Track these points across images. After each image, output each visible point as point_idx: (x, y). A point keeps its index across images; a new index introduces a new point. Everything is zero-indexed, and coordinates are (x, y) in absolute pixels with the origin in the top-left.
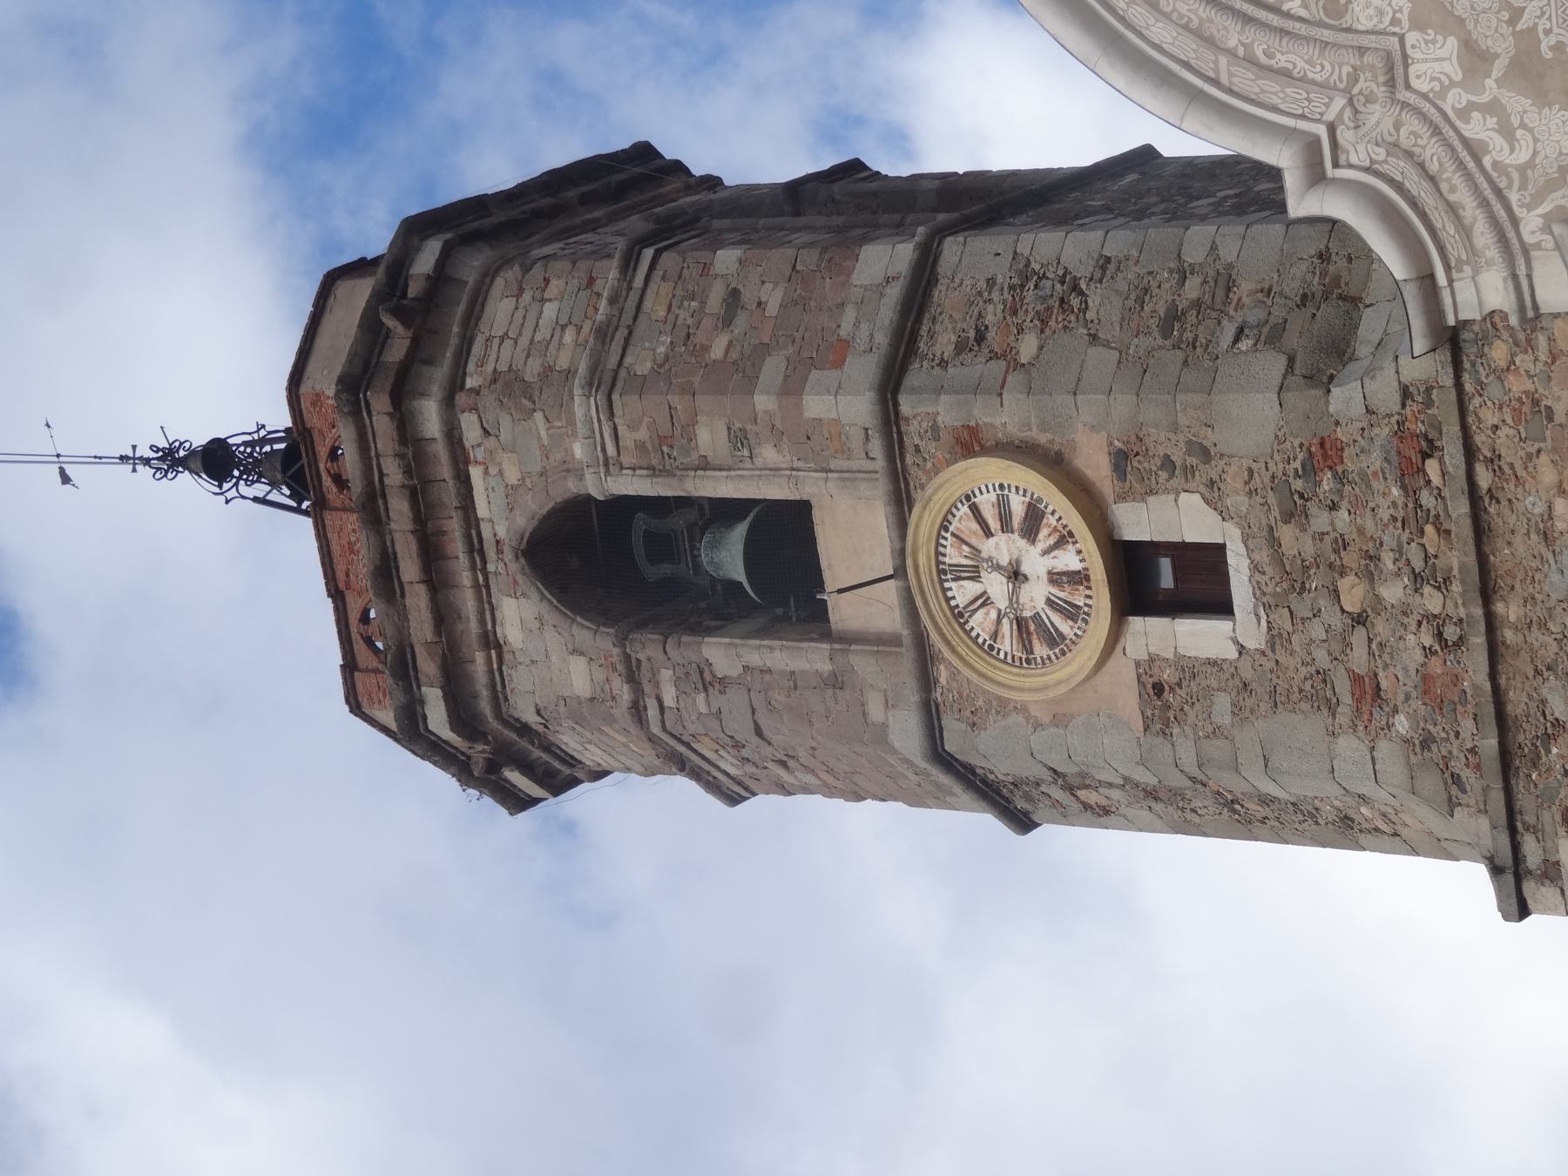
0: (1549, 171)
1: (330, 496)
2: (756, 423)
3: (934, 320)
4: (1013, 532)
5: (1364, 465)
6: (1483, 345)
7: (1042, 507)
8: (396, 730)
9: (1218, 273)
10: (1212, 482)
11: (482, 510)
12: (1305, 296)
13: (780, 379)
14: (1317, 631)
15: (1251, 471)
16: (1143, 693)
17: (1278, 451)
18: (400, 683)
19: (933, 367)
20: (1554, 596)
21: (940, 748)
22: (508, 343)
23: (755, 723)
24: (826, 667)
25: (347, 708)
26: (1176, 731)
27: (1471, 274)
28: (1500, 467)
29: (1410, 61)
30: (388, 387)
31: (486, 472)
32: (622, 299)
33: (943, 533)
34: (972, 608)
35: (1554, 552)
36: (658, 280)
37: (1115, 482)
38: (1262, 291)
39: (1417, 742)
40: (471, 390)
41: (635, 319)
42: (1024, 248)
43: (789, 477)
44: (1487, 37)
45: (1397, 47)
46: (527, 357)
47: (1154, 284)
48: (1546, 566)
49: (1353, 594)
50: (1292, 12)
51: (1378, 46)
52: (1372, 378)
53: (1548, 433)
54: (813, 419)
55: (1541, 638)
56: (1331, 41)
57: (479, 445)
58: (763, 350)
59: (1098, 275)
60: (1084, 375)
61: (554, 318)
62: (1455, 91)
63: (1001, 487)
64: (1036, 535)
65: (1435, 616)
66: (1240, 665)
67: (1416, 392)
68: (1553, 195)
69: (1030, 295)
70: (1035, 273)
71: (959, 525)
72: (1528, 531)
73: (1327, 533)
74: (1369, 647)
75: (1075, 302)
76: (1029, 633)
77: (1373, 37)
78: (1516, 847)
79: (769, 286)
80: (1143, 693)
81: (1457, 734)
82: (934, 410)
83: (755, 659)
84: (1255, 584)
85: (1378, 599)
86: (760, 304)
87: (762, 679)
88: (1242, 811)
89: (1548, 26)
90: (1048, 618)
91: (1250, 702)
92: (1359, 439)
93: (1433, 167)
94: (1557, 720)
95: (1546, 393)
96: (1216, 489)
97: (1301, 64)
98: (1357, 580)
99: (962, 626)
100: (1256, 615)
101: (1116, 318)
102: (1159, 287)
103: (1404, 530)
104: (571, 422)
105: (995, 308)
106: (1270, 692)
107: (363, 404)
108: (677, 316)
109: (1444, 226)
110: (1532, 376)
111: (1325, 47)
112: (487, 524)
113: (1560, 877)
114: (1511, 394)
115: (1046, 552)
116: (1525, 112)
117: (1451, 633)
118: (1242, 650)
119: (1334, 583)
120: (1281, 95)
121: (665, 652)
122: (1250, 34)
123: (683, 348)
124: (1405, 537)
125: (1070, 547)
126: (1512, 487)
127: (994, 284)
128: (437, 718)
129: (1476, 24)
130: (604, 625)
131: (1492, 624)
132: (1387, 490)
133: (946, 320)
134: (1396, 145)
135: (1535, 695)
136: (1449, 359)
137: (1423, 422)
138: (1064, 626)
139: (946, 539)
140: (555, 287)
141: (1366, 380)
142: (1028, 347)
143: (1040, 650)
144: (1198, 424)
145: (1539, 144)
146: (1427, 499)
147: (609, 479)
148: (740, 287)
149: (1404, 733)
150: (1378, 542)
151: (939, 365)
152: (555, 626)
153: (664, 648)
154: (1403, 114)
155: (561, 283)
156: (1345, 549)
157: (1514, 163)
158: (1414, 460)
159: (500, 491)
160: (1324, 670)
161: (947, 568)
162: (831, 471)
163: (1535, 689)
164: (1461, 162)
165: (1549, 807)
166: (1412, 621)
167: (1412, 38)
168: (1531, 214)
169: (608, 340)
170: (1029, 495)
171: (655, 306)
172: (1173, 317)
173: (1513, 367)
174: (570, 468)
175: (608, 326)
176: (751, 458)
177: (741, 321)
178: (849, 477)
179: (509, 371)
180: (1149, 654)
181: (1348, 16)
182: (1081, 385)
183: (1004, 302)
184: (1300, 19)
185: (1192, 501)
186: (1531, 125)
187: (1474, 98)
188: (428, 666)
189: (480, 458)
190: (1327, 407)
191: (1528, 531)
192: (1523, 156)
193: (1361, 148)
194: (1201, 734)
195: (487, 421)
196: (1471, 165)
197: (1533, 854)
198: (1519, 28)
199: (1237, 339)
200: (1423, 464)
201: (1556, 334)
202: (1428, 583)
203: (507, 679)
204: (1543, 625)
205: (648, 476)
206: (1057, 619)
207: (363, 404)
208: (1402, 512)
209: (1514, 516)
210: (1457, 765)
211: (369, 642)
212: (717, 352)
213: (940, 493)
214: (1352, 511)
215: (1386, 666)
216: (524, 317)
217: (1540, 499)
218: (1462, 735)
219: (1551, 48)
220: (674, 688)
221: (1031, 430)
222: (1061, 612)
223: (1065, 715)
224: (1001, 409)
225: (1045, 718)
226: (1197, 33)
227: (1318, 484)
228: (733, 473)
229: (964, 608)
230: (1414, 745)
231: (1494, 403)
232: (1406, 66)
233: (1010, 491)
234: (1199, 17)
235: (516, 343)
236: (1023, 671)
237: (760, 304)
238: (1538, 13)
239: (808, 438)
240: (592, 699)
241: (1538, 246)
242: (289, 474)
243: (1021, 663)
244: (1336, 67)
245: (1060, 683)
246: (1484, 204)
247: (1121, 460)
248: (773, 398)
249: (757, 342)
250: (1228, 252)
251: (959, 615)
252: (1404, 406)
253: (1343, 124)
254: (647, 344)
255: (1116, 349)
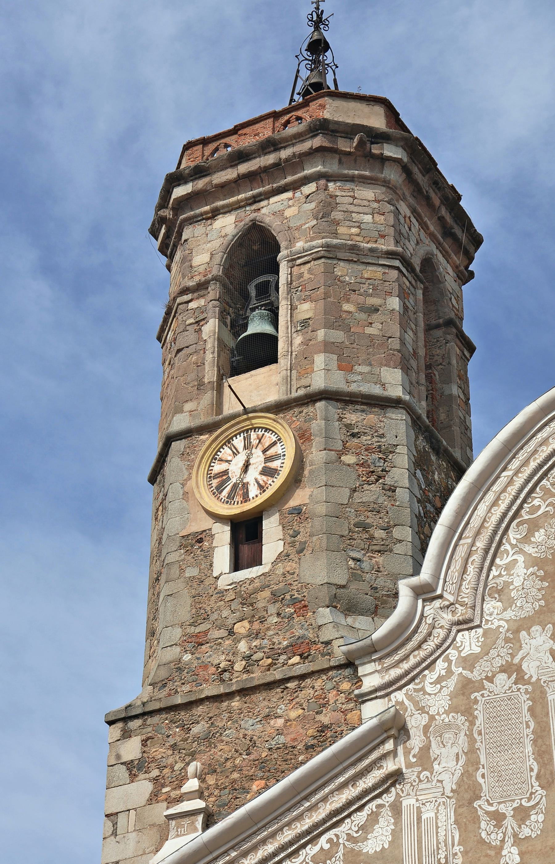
0: (422, 702)
1: (280, 120)
2: (312, 332)
3: (363, 411)
4: (265, 463)
5: (296, 627)
6: (349, 678)
7: (276, 476)
8: (181, 168)
9: (387, 545)
10: (288, 556)
11: (273, 200)
12: (376, 588)
13: (333, 340)
14: (226, 613)
15: (293, 574)
16: (198, 534)
17: (302, 586)
18: (192, 171)
19: (339, 414)
20: (242, 722)
21: (172, 440)
22: (351, 200)
23: (183, 348)
24: (206, 380)
25: (185, 143)
26: (182, 551)
27: (378, 669)
28: (297, 691)
29: (470, 631)
30: (324, 145)
31: (290, 199)
32: (372, 254)
33: (264, 430)
34: (232, 447)
35: (261, 720)
36: (383, 270)
37: (288, 510)
38: (378, 568)
39: (179, 665)
40: (327, 186)
41: (363, 263)
42: (399, 449)
43: (288, 351)
44: (480, 666)
45: (475, 624)
46: (343, 211)
47: (382, 515)
48: (255, 718)
49: (242, 628)
50: (492, 572)
51: (475, 615)
52: (334, 627)
53: (311, 713)
54: (314, 360)
55: (225, 718)
56: (478, 592)
57: (302, 193)
58: (347, 329)
59: (386, 487)
60: (334, 489)
61: (364, 221)
62: (457, 654)
63: (284, 455)
64: (264, 475)
65: (232, 668)
66: (211, 578)
67: (328, 648)
68: (412, 704)
69: (375, 456)
70: (387, 457)
71: (267, 437)
72: (270, 708)
73: (267, 613)
74: (219, 638)
75: (373, 478)
76: (222, 476)
77: (479, 612)
78: (136, 717)
79: (380, 326)
80: (198, 534)
81: (183, 684)
82: (318, 418)
83: (209, 345)
84: (245, 581)
85: (239, 641)
86: (371, 324)
87: (201, 350)
88: (156, 584)
89: (485, 695)
90: (227, 486)
91: (195, 585)
92: (308, 623)
93: (424, 646)
94: (191, 729)
95: (328, 710)
96: (286, 558)
97: (469, 578)
98: (247, 629)
99: (225, 444)
100: (232, 583)
101: (364, 500)
102: (380, 518)
103: (269, 649)
104: (312, 239)
105: (369, 440)
106: (200, 594)
107: (315, 133)
108: (365, 284)
109: (398, 654)
110: (335, 703)
111: (475, 589)
112: (267, 203)
113: (124, 739)
114: (327, 693)
115: (256, 480)
116: (448, 688)
117: (226, 675)
118: (217, 578)
119: (246, 619)
120: (455, 570)
121: (211, 301)
122: (480, 552)
123: (348, 289)
124: (266, 650)
125: (259, 492)
126: (288, 698)
127: (381, 438)
128: (179, 192)
129: (486, 660)
130: (224, 268)
131: (229, 696)
132: (286, 639)
133: (363, 417)
134: (434, 628)
135: (201, 718)
136: (342, 663)
137: (315, 653)
138: (225, 493)
139: (261, 431)
140: (380, 219)
141: (332, 625)
142: (350, 459)
143: (215, 482)
144: (313, 546)
145: (434, 696)
146: (283, 658)
147: (286, 262)
148: (380, 312)
149: (183, 659)
150: (264, 637)
151: (340, 417)
152: (223, 243)
153: (213, 300)
154: (445, 630)
155: (382, 221)
156: (260, 622)
157: (426, 685)
158: (299, 650)
159: (282, 207)
160: (209, 618)
161: (249, 433)
162: (291, 371)
163: (203, 718)
164: (425, 660)
165: (154, 730)
166: (231, 657)
167: (480, 631)
168: (404, 695)
169: (352, 251)
170: (281, 469)
171: (369, 272)
172: (365, 527)
173: (339, 693)
174: (291, 242)
175: (358, 250)
176: (297, 331)
177: (363, 316)
178: (288, 381)
179: (336, 204)
180: (214, 534)
181: (490, 599)
182: (330, 488)
183: (372, 444)
184: (488, 576)
185: (280, 547)
186: (442, 691)
187: (453, 663)
188: (201, 184)
189: (296, 195)
190: (321, 607)
191: (270, 708)
192: (429, 689)
193: (432, 611)
194: (181, 563)
195: (312, 196)
196: (424, 665)
197: (135, 724)
198: (484, 681)
199: (354, 559)
200: (298, 655)
201: (354, 712)
202: (247, 663)
203: (200, 223)
204: (230, 719)
205: (287, 281)
206: (228, 489)
207: (315, 133)
208: (277, 647)
209: (276, 700)
210: (170, 685)
211: (216, 149)
212: (347, 307)
213: (280, 426)
214: (277, 624)
215: (211, 647)
216: (365, 206)
217: (283, 712)
218: (183, 686)
219: (476, 697)
220: (196, 307)
221: (310, 466)
222: (231, 490)
223: (188, 498)
224: (318, 450)
225: (186, 489)
226: (482, 526)
227: (288, 606)
228: (289, 323)
229: (232, 444)
230: (178, 664)
231: (324, 686)
232: (468, 629)
233: (282, 460)
234: (489, 526)
235: (351, 204)
236: (205, 475)
237: (371, 324)
238: (491, 690)
239: (306, 358)
240: (191, 266)
241: (390, 700)
242: (309, 87)
243: (209, 474)
244: (467, 596)
245: (200, 494)
246: (407, 673)
247: (298, 511)
248: (322, 339)
249: (351, 326)
250: (398, 549)
251: (229, 441)
252: (322, 643)
253: (442, 602)
254: (350, 271)
255: (349, 502)
